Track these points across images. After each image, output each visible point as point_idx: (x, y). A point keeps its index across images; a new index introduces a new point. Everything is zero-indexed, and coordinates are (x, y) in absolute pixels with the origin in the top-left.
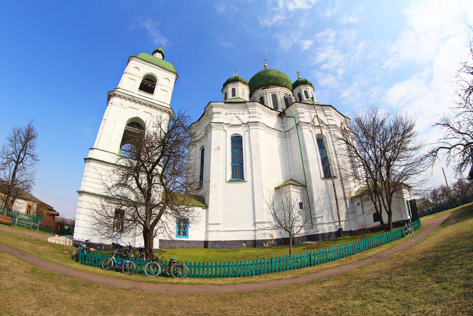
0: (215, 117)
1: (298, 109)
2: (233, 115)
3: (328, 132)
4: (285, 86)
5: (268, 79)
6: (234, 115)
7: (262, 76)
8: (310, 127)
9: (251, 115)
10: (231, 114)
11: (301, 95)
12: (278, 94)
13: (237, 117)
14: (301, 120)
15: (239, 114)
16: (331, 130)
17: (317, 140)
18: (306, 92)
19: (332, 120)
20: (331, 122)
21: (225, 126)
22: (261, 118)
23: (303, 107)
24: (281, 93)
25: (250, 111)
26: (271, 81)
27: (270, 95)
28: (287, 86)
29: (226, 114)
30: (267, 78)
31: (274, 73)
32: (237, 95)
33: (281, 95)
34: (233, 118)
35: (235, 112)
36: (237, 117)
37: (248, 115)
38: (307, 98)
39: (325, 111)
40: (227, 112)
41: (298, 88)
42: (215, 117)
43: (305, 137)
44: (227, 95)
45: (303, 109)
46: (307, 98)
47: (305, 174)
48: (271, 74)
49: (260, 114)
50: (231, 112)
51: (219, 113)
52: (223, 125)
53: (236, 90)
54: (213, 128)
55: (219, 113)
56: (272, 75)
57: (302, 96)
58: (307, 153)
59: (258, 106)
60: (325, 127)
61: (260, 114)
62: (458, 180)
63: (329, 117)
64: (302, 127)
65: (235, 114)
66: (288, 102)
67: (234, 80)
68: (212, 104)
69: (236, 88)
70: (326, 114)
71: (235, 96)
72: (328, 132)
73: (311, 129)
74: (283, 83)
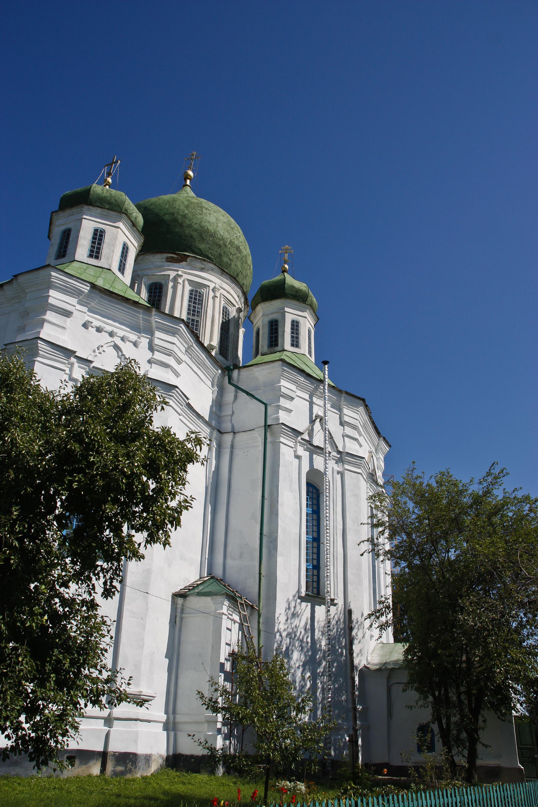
0: (49, 322)
1: (283, 383)
2: (104, 338)
3: (338, 472)
4: (235, 275)
5: (195, 234)
6: (110, 339)
7: (180, 217)
8: (298, 444)
9: (158, 356)
10: (99, 330)
11: (280, 330)
12: (211, 294)
13: (116, 347)
14: (283, 417)
15: (123, 339)
16: (347, 467)
17: (308, 484)
18: (295, 326)
19: (355, 439)
20: (351, 447)
21: (76, 365)
22: (177, 374)
23: (295, 382)
24: (218, 294)
25: (157, 342)
26: (202, 246)
27: (188, 288)
28: (240, 279)
29: (85, 325)
30: (196, 230)
31: (220, 225)
32: (108, 258)
33: (217, 300)
34: (105, 348)
35: (115, 330)
36: (116, 347)
37: (149, 355)
38: (292, 345)
39: (346, 411)
40: (91, 319)
41: (276, 304)
42: (49, 322)
43: (281, 469)
44: (70, 246)
45: (293, 387)
46: (292, 345)
47: (260, 574)
48: (209, 222)
49: (179, 361)
50: (103, 325)
51: (67, 314)
52: (73, 360)
53: (107, 238)
54: (38, 359)
55: (67, 314)
56: (211, 228)
57: (280, 333)
58: (277, 514)
59: (182, 337)
60: (334, 454)
61: (179, 361)
62: (476, 488)
63: (349, 431)
64: (282, 440)
65: (111, 334)
66: (228, 329)
67: (110, 203)
68: (53, 274)
69: (109, 232)
70: (346, 419)
71: (97, 257)
72: (338, 472)
73: (301, 451)
74: (233, 264)
